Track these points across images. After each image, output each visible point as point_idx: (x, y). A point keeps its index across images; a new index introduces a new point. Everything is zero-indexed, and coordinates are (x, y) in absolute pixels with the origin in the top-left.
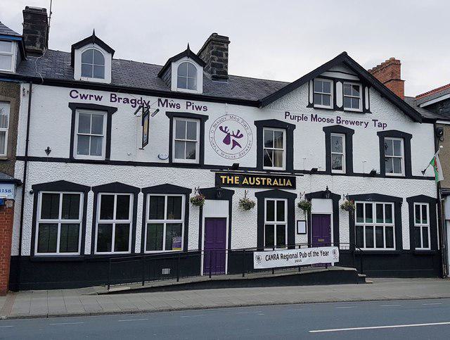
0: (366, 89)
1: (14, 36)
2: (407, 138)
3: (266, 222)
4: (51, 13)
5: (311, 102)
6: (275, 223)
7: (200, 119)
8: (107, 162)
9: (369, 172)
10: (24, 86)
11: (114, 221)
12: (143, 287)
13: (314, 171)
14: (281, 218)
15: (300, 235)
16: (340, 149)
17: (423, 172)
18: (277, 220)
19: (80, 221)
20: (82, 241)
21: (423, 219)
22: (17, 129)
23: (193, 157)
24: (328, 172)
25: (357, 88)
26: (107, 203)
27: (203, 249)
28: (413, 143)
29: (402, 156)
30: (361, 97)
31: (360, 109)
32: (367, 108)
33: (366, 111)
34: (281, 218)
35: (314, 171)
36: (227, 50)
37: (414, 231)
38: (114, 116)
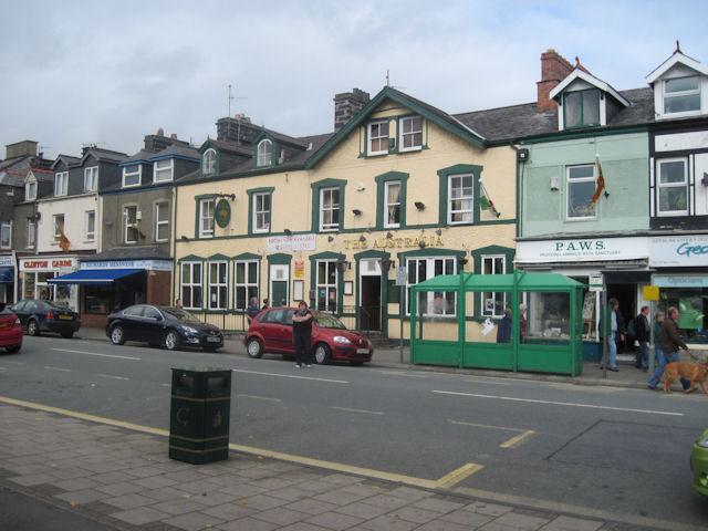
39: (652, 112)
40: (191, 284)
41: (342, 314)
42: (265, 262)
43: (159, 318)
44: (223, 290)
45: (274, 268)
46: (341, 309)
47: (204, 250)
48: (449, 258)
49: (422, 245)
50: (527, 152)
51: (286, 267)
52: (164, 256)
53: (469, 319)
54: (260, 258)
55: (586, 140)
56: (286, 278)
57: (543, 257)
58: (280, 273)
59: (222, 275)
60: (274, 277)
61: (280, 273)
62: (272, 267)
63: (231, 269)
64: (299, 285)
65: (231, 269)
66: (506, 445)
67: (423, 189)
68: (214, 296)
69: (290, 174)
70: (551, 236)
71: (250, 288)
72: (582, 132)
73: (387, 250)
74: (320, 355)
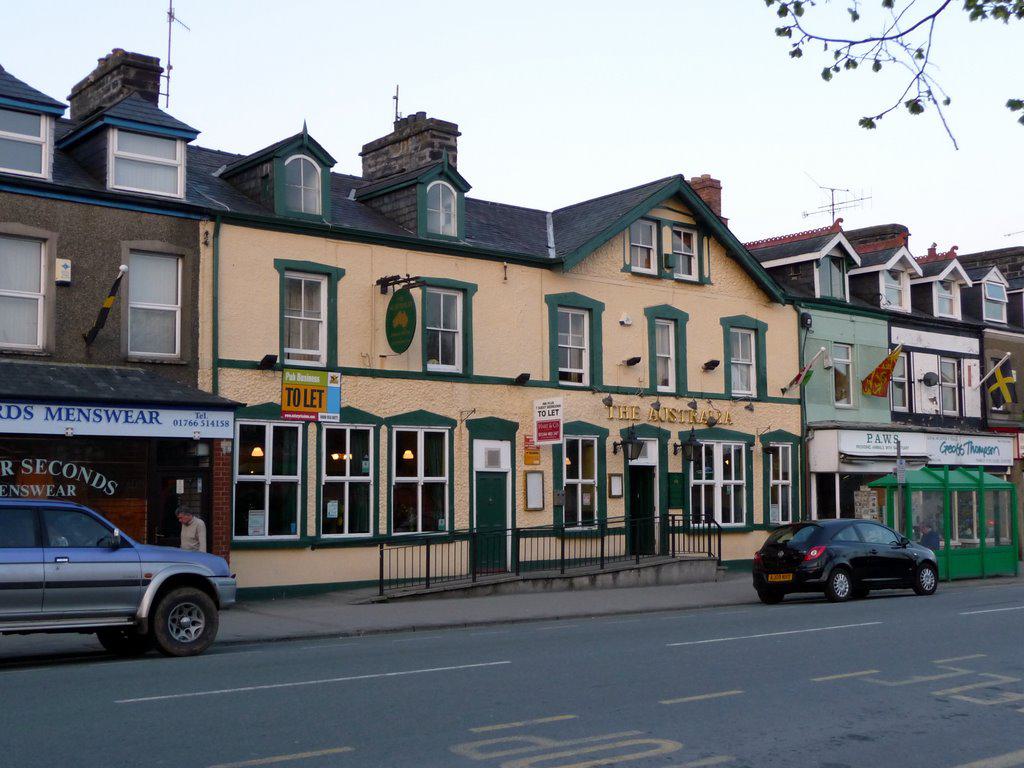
0: (705, 240)
1: (43, 104)
2: (759, 329)
3: (566, 481)
4: (170, 67)
5: (628, 263)
6: (781, 482)
7: (328, 275)
8: (467, 377)
9: (259, 358)
10: (206, 227)
11: (733, 481)
12: (428, 591)
13: (523, 380)
14: (738, 477)
15: (614, 500)
16: (746, 355)
17: (784, 391)
18: (583, 477)
19: (298, 478)
20: (374, 516)
21: (778, 471)
22: (197, 307)
23: (448, 359)
24: (552, 384)
25: (688, 237)
26: (407, 441)
27: (475, 526)
28: (690, 328)
29: (586, 345)
30: (695, 253)
31: (694, 277)
32: (706, 275)
33: (702, 282)
34: (587, 474)
35: (523, 380)
36: (454, 149)
37: (771, 495)
38: (342, 285)
39: (104, 182)
40: (421, 478)
41: (604, 532)
42: (462, 433)
43: (856, 552)
44: (359, 491)
45: (482, 447)
46: (603, 522)
47: (389, 399)
48: (588, 437)
49: (711, 423)
50: (808, 316)
51: (504, 447)
52: (175, 394)
53: (679, 530)
54: (452, 423)
55: (848, 317)
56: (505, 466)
57: (858, 450)
58: (493, 457)
59: (587, 462)
60: (480, 465)
61: (493, 457)
62: (477, 443)
63: (383, 445)
64: (534, 481)
65: (383, 445)
66: (349, 749)
67: (705, 342)
68: (587, 501)
69: (515, 270)
70: (864, 425)
71: (352, 485)
72: (259, 222)
73: (665, 427)
74: (842, 584)
